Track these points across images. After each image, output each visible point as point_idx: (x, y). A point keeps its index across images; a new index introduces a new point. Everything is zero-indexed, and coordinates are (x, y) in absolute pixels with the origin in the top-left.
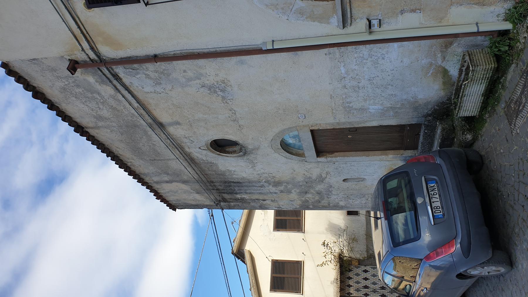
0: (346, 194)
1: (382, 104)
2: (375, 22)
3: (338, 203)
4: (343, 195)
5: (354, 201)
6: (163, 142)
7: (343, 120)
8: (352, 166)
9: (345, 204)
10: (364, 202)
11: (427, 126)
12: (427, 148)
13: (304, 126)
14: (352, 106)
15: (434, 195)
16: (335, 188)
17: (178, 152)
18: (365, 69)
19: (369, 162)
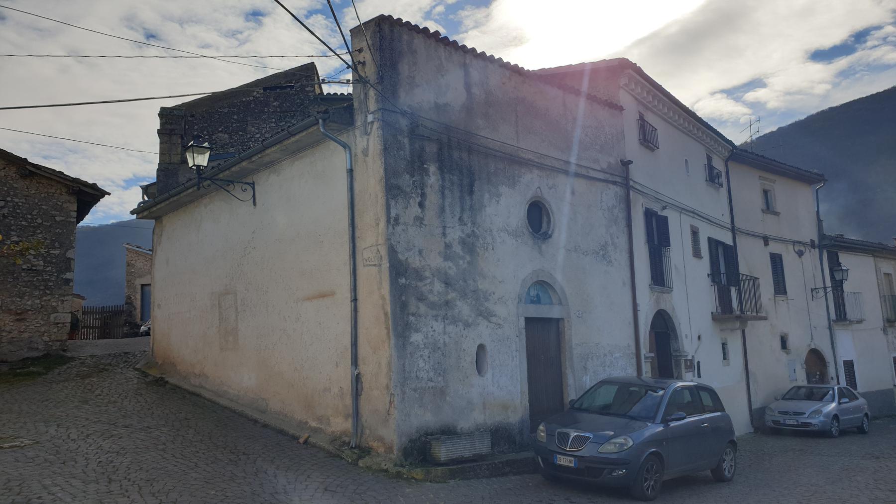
2: (338, 363)
3: (417, 331)
4: (444, 342)
10: (422, 374)
19: (519, 379)
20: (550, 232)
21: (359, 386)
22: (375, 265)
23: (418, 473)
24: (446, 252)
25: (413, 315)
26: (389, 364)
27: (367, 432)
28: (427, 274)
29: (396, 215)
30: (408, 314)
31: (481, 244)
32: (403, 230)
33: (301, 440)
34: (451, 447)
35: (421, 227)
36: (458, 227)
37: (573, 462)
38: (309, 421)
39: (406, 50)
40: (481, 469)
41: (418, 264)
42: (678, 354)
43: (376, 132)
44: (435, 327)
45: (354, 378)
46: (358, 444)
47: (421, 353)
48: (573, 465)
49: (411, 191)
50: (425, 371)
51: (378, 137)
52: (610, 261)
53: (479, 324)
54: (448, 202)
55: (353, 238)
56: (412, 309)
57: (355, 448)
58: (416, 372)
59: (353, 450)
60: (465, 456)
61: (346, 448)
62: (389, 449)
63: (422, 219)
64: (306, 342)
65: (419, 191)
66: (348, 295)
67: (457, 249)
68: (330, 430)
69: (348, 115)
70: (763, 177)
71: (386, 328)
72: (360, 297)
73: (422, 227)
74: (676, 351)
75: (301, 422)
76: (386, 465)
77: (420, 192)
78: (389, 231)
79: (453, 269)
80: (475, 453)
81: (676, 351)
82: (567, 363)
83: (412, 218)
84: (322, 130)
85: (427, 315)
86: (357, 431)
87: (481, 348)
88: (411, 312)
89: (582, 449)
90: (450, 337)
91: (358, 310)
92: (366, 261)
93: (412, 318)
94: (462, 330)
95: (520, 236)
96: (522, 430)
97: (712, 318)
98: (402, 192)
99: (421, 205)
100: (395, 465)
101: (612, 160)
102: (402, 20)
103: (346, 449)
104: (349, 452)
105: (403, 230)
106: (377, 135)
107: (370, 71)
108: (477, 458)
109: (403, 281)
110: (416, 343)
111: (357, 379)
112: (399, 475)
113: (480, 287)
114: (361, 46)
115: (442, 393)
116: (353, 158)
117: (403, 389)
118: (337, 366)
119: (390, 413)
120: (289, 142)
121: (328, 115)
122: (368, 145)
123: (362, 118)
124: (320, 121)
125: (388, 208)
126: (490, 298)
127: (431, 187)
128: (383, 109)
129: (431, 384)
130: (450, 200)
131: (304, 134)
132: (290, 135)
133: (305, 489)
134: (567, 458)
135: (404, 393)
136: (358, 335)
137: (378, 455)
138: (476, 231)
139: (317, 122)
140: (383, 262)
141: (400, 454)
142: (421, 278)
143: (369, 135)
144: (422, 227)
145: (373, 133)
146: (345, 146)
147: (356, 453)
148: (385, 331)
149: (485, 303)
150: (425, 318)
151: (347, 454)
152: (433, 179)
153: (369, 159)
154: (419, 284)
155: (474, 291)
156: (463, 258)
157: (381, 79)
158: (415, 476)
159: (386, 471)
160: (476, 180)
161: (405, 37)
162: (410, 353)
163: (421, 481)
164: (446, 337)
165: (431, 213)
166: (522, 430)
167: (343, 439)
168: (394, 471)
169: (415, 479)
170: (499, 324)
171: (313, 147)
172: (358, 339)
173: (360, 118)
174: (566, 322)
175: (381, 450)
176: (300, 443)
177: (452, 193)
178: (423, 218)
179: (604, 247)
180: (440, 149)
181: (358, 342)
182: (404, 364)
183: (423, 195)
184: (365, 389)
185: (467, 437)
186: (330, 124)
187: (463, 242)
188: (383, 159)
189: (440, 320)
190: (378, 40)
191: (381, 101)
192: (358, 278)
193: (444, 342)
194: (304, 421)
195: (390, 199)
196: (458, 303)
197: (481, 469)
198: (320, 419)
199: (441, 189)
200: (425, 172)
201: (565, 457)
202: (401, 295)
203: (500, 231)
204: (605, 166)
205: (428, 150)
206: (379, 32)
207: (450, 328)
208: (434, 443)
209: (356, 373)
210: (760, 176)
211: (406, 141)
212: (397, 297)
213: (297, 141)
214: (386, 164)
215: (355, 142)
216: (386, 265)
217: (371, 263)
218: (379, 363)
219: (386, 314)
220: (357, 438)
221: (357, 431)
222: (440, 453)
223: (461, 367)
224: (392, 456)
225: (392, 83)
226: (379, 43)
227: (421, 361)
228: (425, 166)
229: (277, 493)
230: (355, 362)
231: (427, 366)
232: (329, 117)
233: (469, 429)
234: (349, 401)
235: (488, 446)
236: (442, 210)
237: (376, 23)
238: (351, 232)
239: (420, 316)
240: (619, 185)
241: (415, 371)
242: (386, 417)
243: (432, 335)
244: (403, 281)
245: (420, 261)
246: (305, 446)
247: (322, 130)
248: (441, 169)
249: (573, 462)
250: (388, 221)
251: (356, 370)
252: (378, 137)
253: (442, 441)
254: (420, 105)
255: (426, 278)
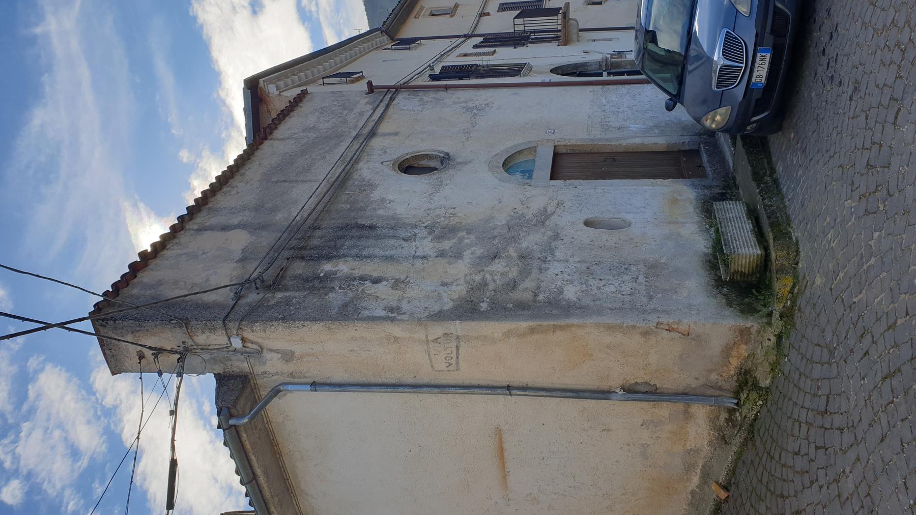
0: (584, 261)
1: (644, 124)
2: (604, 427)
3: (561, 292)
4: (579, 262)
5: (602, 283)
6: (329, 172)
7: (598, 136)
8: (605, 192)
9: (579, 293)
10: (627, 288)
11: (706, 143)
12: (719, 167)
13: (548, 141)
14: (611, 125)
15: (762, 64)
16: (565, 241)
17: (340, 170)
18: (624, 100)
19: (635, 187)
20: (442, 155)
21: (643, 389)
22: (457, 347)
23: (782, 285)
24: (451, 256)
25: (536, 295)
26: (610, 328)
27: (714, 377)
28: (478, 278)
29: (385, 310)
30: (535, 301)
31: (445, 220)
32: (409, 302)
33: (723, 495)
34: (739, 242)
35: (409, 282)
36: (417, 242)
37: (764, 54)
38: (690, 489)
39: (153, 291)
40: (771, 205)
41: (463, 287)
42: (604, 64)
43: (257, 334)
44: (557, 271)
45: (629, 395)
46: (732, 395)
47: (594, 288)
48: (768, 56)
49: (352, 291)
50: (622, 285)
51: (264, 331)
52: (487, 105)
53: (556, 225)
54: (377, 251)
55: (416, 387)
56: (527, 296)
57: (739, 400)
58: (624, 295)
59: (742, 401)
60: (752, 228)
61: (738, 414)
62: (744, 334)
63: (397, 281)
64: (570, 487)
65: (355, 283)
66: (501, 401)
67: (447, 244)
68: (706, 449)
69: (232, 381)
70: (416, 15)
71: (553, 332)
72: (504, 380)
73: (409, 281)
74: (600, 66)
75: (691, 504)
76: (770, 340)
77: (358, 282)
78: (407, 319)
79: (474, 250)
80: (745, 217)
81: (600, 66)
82: (613, 144)
83: (394, 291)
84: (246, 420)
85: (539, 279)
86: (712, 396)
87: (588, 223)
88: (531, 298)
89: (741, 39)
90: (573, 255)
91: (525, 385)
92: (451, 364)
93: (541, 297)
94: (563, 243)
95: (442, 182)
96: (704, 186)
97: (564, 45)
98: (353, 302)
99: (376, 281)
100: (769, 324)
101: (364, 101)
102: (108, 291)
103: (740, 414)
104: (744, 410)
105: (409, 302)
106: (262, 333)
107: (169, 338)
108: (753, 215)
109: (484, 306)
110: (579, 293)
111: (632, 391)
112: (787, 315)
113: (504, 222)
114: (136, 354)
115: (653, 268)
116: (296, 380)
117: (649, 311)
118: (608, 430)
119: (686, 333)
120: (266, 488)
121: (223, 408)
122: (277, 351)
123: (238, 360)
124: (232, 422)
125: (374, 319)
126: (520, 212)
127: (353, 269)
128: (224, 320)
129: (641, 279)
130: (378, 250)
131: (253, 457)
132: (254, 481)
133: (827, 449)
134: (757, 65)
135: (655, 310)
136: (563, 387)
137: (752, 355)
138: (426, 224)
139: (233, 427)
140: (453, 331)
141: (751, 318)
142: (484, 284)
143: (262, 348)
144: (409, 281)
145: (260, 341)
146: (276, 392)
147: (748, 395)
148: (558, 333)
149: (527, 217)
150: (542, 281)
151: (748, 411)
152: (343, 267)
153: (298, 349)
154: (491, 286)
155: (509, 229)
156: (461, 240)
157: (184, 323)
158: (788, 289)
159: (779, 337)
160: (356, 222)
161: (135, 291)
162: (593, 301)
163: (796, 277)
164: (571, 260)
165: (391, 271)
166: (704, 186)
167: (722, 424)
168: (780, 323)
169: (793, 287)
170: (558, 204)
171: (281, 455)
172: (568, 387)
173: (237, 363)
174: (559, 143)
175: (744, 350)
176: (728, 497)
177: (368, 247)
178: (396, 279)
179: (469, 109)
180: (303, 258)
181: (574, 387)
182: (610, 309)
183: (363, 278)
184: (647, 378)
185: (723, 225)
186: (238, 407)
187: (439, 238)
188: (298, 323)
189: (547, 266)
190: (125, 323)
191: (213, 323)
192: (474, 382)
193: (579, 262)
194: (690, 497)
195: (360, 316)
196: (524, 245)
197: (771, 205)
198: (689, 468)
199: (359, 259)
200: (329, 276)
201: (756, 69)
202: (505, 309)
203: (431, 201)
204: (369, 107)
205: (299, 272)
206: (115, 321)
207: (559, 254)
208: (733, 267)
209: (622, 392)
210: (415, 17)
211: (279, 295)
212: (507, 313)
213: (266, 473)
214: (306, 320)
215: (273, 375)
216: (457, 327)
217: (454, 356)
218: (608, 347)
219: (532, 331)
220: (722, 396)
221: (712, 396)
222: (750, 256)
223: (616, 245)
224: (753, 331)
225: (192, 308)
226: (131, 321)
227: (606, 289)
228: (322, 275)
229: (839, 496)
230: (603, 394)
231: (613, 283)
232: (228, 408)
233: (707, 239)
234: (664, 410)
235: (735, 204)
236: (390, 259)
237: (102, 325)
238: (406, 390)
239: (539, 287)
240: (396, 95)
241: (622, 296)
242: (693, 339)
243: (568, 275)
244: (484, 306)
245: (458, 285)
246: (733, 488)
247: (246, 420)
248: (329, 258)
249: (764, 54)
250: (392, 319)
251: (616, 393)
252: (264, 331)
253: (731, 253)
254: (234, 278)
255: (483, 279)
